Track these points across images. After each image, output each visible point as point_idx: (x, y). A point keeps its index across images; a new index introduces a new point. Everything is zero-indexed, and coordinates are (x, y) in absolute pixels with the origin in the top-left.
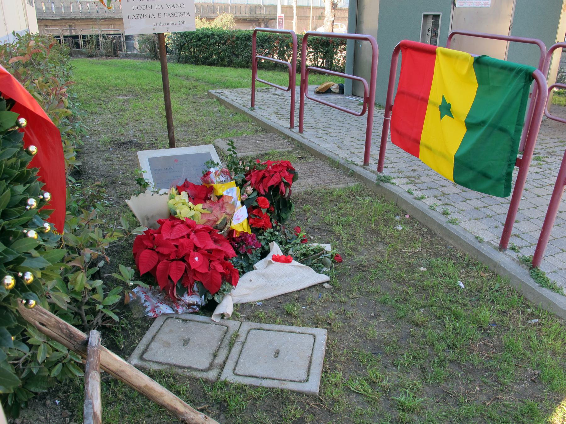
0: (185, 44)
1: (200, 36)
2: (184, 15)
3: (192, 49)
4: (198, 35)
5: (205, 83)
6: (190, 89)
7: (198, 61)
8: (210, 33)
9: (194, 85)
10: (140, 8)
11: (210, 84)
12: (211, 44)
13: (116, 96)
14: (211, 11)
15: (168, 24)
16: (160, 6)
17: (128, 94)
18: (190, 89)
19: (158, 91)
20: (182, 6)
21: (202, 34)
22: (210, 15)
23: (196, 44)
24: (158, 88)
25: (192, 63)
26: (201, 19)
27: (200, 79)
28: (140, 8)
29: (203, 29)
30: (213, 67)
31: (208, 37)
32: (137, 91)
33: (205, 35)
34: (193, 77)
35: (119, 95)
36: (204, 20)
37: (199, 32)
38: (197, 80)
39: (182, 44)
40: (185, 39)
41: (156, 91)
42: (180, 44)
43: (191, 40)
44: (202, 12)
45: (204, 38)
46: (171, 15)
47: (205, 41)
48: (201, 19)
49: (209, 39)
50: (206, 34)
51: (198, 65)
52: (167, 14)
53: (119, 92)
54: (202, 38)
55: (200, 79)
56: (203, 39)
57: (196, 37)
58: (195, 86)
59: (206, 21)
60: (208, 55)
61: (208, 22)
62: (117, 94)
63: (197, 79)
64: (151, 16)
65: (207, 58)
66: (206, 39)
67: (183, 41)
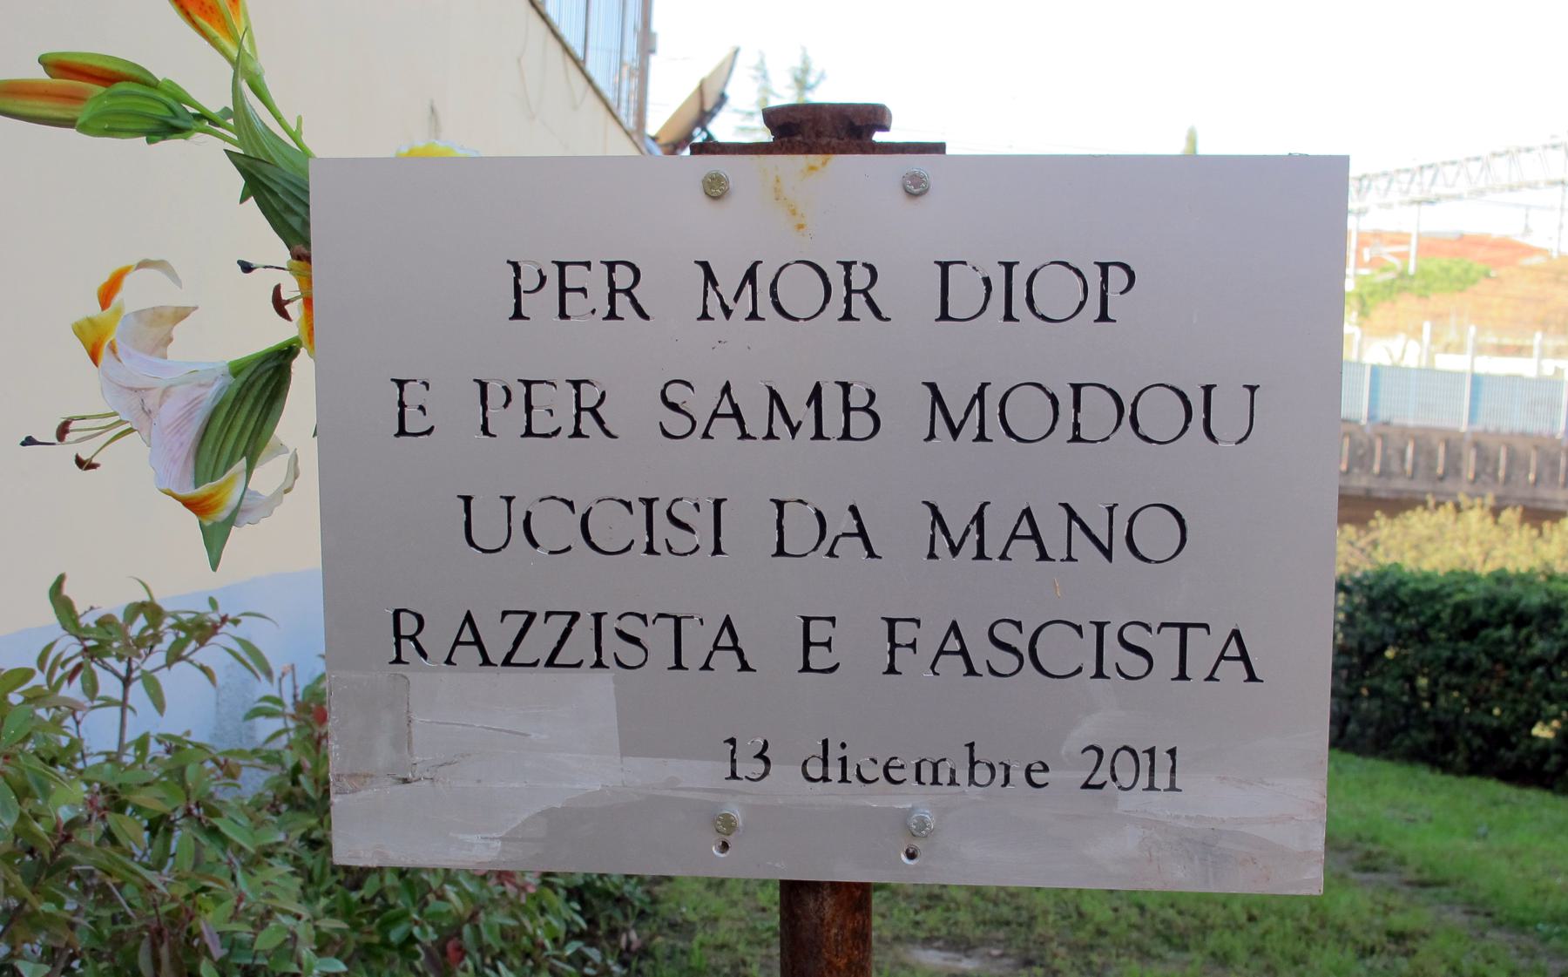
0: (1384, 647)
1: (1479, 612)
2: (1167, 661)
3: (1423, 682)
4: (1463, 609)
5: (1472, 908)
6: (1367, 952)
7: (1449, 745)
8: (1535, 600)
9: (1398, 922)
10: (556, 527)
11: (1498, 925)
12: (1537, 662)
13: (912, 940)
14: (1554, 475)
15: (930, 772)
16: (841, 522)
17: (983, 942)
18: (1367, 952)
19: (1168, 940)
20: (1156, 534)
21: (1491, 602)
22: (1544, 492)
23: (1446, 654)
24: (1167, 923)
25: (1416, 756)
26: (1496, 512)
27: (1444, 883)
28: (556, 527)
29: (1501, 578)
30: (1533, 795)
31: (1521, 620)
32: (1039, 929)
33: (1503, 614)
34: (1401, 861)
35: (928, 942)
36: (1508, 515)
37: (1475, 592)
38: (1424, 885)
39: (1370, 647)
40: (1391, 622)
41: (1160, 948)
42: (1361, 645)
43: (1424, 628)
44: (1508, 477)
45: (1500, 626)
46: (981, 651)
47: (1501, 641)
48: (1496, 512)
49: (1524, 632)
50: (1512, 605)
51: (1446, 768)
52: (930, 640)
53: (932, 918)
54: (1484, 624)
55: (1444, 883)
56: (1492, 634)
57: (1454, 617)
58: (1399, 937)
59: (1523, 521)
60: (1508, 720)
61: (1528, 532)
62: (921, 934)
63: (1427, 876)
64: (697, 642)
65: (1499, 737)
66: (1507, 632)
67: (1377, 630)
